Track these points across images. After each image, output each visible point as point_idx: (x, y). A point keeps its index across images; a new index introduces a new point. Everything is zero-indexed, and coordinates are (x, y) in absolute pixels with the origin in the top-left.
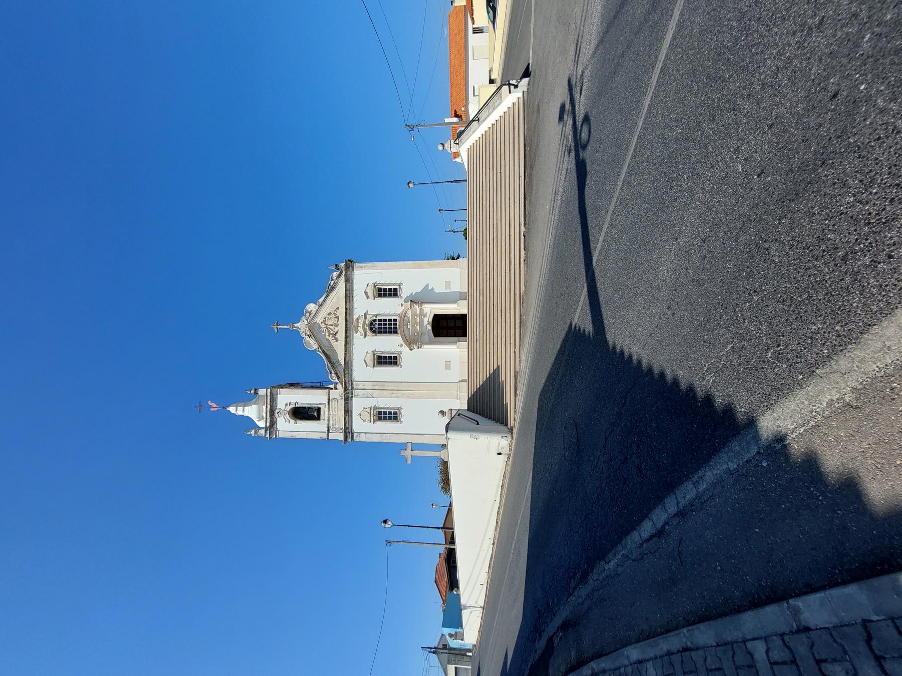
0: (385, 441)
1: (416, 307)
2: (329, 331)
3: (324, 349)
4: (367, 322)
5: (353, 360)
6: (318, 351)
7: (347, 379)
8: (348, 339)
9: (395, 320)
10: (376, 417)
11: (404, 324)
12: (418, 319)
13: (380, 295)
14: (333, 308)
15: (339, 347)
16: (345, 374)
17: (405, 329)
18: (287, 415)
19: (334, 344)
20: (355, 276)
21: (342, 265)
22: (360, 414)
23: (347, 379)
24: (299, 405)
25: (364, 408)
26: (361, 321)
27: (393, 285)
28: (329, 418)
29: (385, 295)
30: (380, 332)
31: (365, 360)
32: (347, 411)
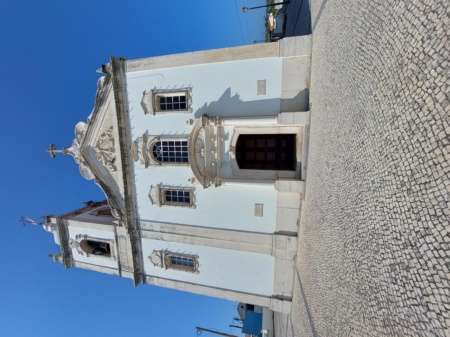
0: (180, 289)
1: (212, 124)
2: (105, 158)
3: (103, 180)
4: (148, 146)
5: (136, 195)
6: (96, 182)
7: (132, 217)
8: (127, 169)
9: (185, 143)
10: (169, 262)
11: (196, 151)
12: (216, 142)
13: (163, 108)
14: (106, 127)
15: (118, 176)
16: (128, 212)
17: (198, 158)
18: (80, 248)
19: (113, 174)
20: (128, 82)
21: (109, 65)
22: (150, 257)
23: (132, 217)
24: (88, 239)
25: (154, 251)
26: (141, 144)
27: (178, 91)
28: (118, 255)
29: (170, 108)
30: (166, 160)
31: (150, 196)
32: (136, 252)
